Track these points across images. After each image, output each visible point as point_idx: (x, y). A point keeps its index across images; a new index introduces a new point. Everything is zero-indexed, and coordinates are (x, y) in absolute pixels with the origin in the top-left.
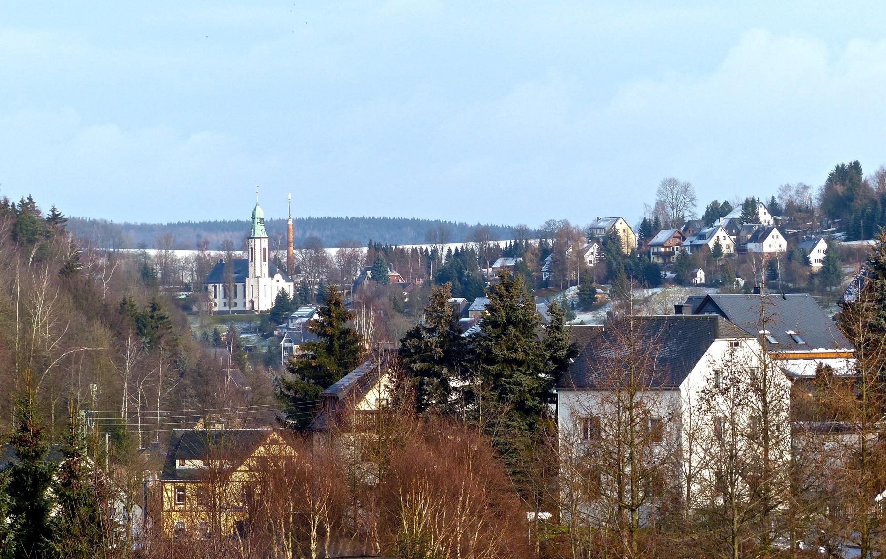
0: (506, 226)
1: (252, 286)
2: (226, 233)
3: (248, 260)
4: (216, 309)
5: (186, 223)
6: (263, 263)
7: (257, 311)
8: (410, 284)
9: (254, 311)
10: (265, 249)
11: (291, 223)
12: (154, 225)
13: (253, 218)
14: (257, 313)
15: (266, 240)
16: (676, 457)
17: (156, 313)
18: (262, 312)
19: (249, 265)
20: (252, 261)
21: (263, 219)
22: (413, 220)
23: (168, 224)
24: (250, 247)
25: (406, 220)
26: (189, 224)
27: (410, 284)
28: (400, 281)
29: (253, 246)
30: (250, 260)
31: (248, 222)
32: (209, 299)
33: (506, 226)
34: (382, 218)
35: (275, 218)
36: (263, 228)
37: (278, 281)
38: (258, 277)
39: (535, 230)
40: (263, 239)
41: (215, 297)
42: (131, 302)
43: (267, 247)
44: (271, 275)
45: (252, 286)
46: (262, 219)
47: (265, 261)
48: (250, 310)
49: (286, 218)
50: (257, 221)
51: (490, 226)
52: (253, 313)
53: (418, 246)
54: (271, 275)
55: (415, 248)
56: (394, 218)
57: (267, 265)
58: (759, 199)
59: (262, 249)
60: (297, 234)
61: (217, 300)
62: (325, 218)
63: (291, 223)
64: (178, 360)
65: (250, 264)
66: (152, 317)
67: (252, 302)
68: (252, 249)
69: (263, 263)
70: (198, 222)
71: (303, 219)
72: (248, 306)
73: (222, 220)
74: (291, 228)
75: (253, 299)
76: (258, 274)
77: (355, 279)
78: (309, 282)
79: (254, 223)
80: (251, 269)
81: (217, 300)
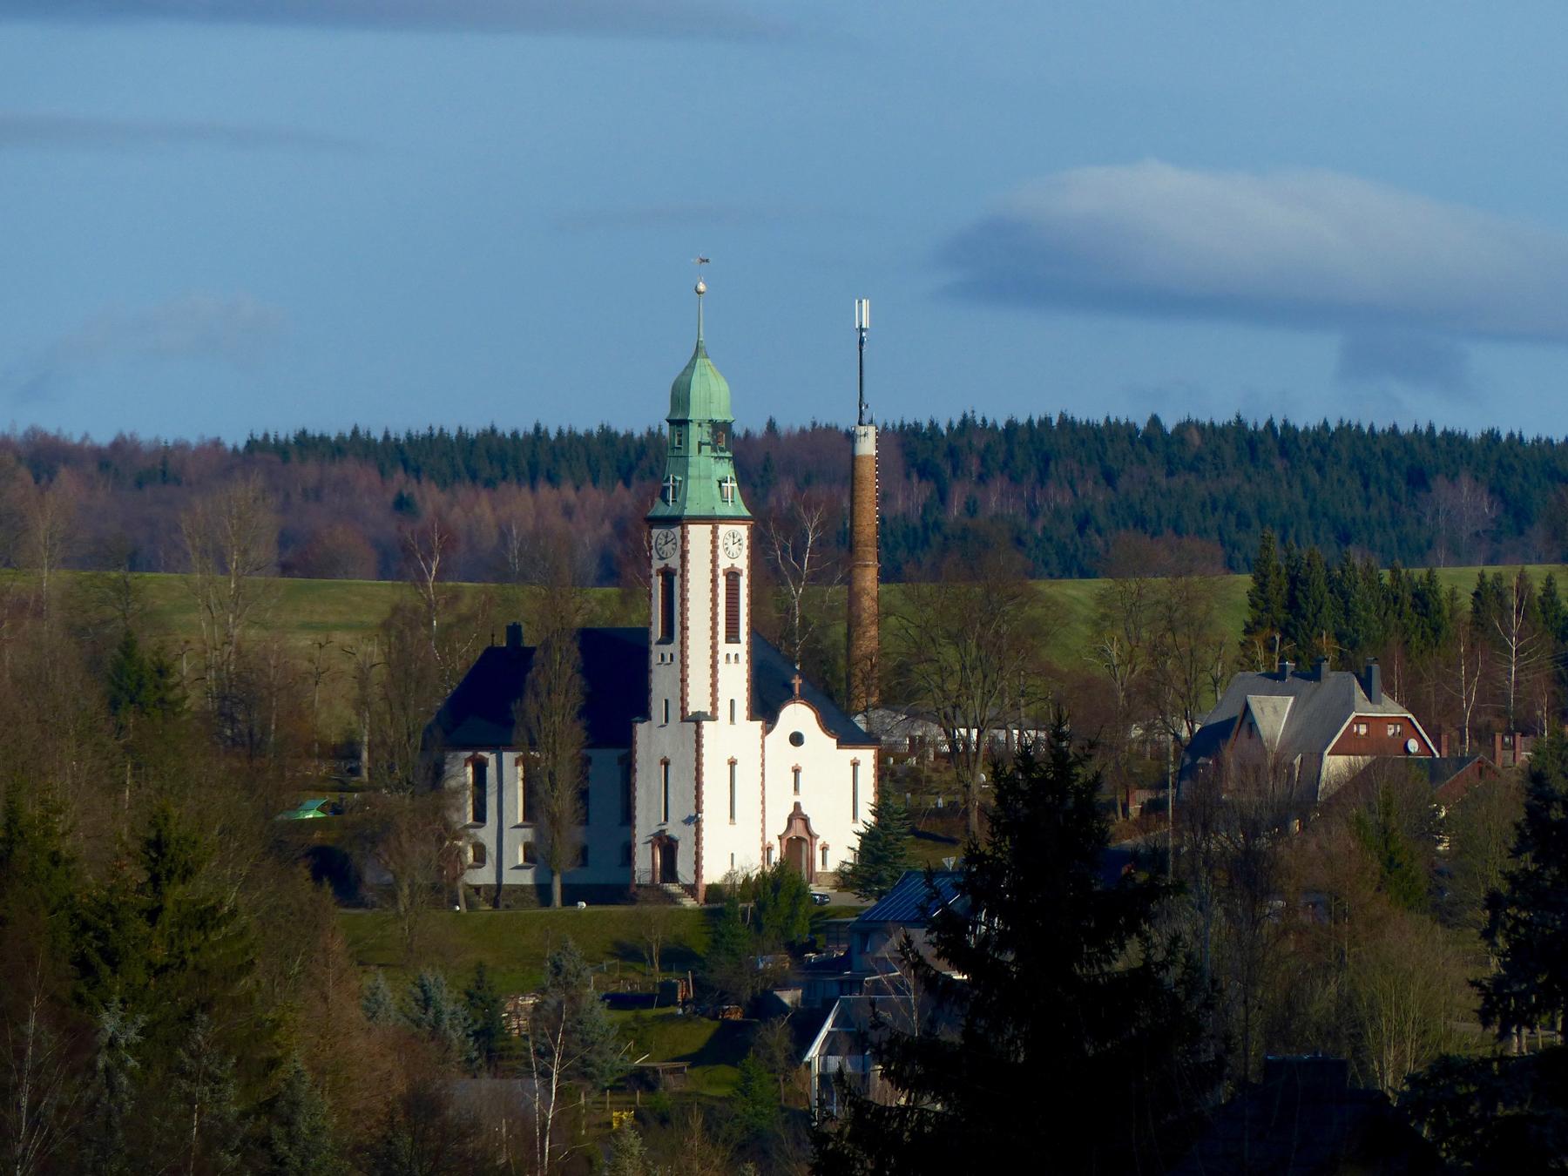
0: (1349, 425)
1: (666, 763)
2: (544, 490)
3: (645, 633)
4: (484, 876)
5: (341, 438)
6: (724, 648)
7: (691, 890)
8: (1462, 761)
9: (673, 888)
10: (733, 576)
11: (867, 446)
12: (182, 447)
13: (680, 425)
14: (689, 903)
15: (743, 531)
16: (1488, 498)
17: (176, 893)
18: (713, 890)
19: (655, 658)
20: (668, 636)
21: (726, 426)
22: (1491, 438)
23: (252, 445)
24: (657, 564)
25: (1453, 440)
26: (355, 447)
27: (1462, 761)
28: (1413, 745)
29: (674, 562)
30: (657, 631)
31: (653, 437)
32: (447, 826)
33: (1349, 425)
34: (1333, 426)
35: (793, 420)
36: (726, 470)
37: (796, 739)
38: (698, 719)
39: (1306, 428)
40: (723, 529)
41: (480, 817)
42: (48, 834)
43: (742, 563)
44: (765, 707)
45: (666, 763)
46: (720, 429)
47: (732, 636)
48: (651, 887)
49: (846, 421)
50: (696, 434)
51: (1457, 432)
52: (672, 898)
53: (1509, 573)
54: (765, 707)
55: (1489, 578)
56: (1394, 430)
57: (744, 657)
58: (1521, 432)
59: (722, 581)
60: (899, 504)
61: (487, 835)
62: (1046, 422)
63: (867, 446)
64: (277, 1131)
65: (656, 652)
66: (153, 915)
67: (668, 847)
68: (668, 574)
69: (724, 648)
70: (399, 431)
71: (933, 426)
72: (645, 861)
73: (526, 427)
74: (868, 471)
75: (673, 830)
76: (698, 701)
77: (1185, 734)
78: (953, 745)
79: (683, 440)
80: (661, 683)
81: (487, 835)
